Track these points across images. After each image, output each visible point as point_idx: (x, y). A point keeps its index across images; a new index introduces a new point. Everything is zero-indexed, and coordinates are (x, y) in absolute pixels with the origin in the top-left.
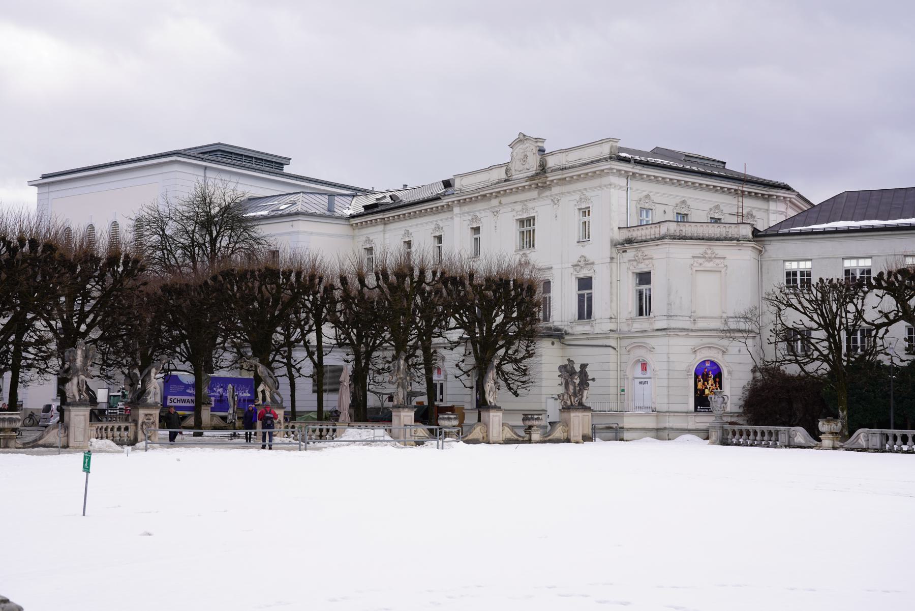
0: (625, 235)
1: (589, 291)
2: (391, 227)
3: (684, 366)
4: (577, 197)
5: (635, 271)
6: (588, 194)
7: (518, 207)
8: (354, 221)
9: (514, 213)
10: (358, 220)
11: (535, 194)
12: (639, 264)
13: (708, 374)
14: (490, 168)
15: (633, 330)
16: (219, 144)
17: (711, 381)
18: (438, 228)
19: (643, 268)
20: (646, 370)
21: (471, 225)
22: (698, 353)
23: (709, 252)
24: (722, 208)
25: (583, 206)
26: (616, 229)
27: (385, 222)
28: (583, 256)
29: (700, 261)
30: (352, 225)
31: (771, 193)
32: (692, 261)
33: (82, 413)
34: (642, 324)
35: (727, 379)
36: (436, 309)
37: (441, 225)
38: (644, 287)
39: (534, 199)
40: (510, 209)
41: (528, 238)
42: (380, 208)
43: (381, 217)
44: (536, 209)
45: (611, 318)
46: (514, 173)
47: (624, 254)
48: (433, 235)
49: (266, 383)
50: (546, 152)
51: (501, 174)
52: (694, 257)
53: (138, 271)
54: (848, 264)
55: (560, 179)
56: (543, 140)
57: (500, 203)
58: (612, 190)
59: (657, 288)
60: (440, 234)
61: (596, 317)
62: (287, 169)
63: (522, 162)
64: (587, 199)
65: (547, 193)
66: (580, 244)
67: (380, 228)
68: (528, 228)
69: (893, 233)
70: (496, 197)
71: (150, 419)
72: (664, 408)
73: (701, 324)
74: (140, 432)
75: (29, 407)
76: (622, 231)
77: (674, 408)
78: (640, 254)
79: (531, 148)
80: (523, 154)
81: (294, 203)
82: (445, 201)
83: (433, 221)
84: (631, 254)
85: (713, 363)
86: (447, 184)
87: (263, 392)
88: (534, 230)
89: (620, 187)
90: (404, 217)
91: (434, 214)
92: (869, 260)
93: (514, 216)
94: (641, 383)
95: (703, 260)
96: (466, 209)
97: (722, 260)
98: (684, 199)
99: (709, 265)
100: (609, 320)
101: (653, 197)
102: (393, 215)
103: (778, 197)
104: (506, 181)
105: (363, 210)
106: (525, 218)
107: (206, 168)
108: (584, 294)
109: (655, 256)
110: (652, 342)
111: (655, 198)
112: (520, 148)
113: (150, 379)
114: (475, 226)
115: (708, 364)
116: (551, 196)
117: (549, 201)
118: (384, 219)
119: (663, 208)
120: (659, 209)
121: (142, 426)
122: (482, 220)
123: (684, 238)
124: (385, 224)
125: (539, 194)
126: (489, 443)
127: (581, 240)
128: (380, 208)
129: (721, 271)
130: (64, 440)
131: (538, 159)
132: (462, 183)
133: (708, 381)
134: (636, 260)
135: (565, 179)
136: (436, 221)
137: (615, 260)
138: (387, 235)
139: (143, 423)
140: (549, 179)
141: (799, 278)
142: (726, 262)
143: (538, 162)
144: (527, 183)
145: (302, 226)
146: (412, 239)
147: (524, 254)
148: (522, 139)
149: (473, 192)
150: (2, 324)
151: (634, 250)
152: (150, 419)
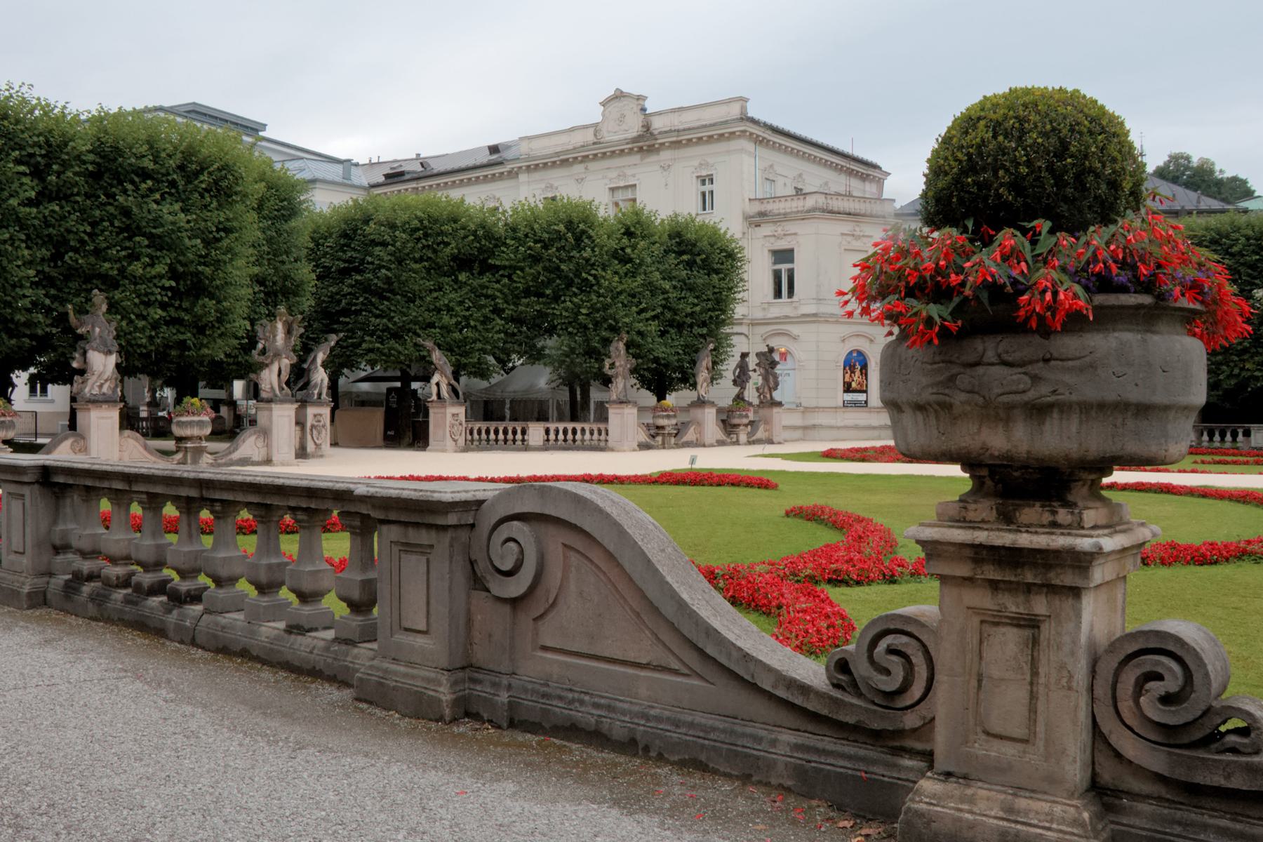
0: (756, 208)
1: (789, 266)
4: (696, 163)
6: (710, 161)
7: (614, 174)
11: (636, 158)
13: (855, 365)
14: (572, 130)
15: (770, 316)
16: (194, 103)
17: (858, 373)
19: (782, 245)
22: (846, 342)
23: (857, 229)
25: (704, 173)
26: (747, 200)
29: (849, 239)
33: (286, 413)
34: (782, 308)
36: (88, 300)
38: (784, 267)
43: (414, 185)
46: (606, 134)
49: (443, 373)
51: (589, 137)
55: (672, 143)
56: (643, 98)
59: (801, 268)
62: (261, 133)
64: (707, 164)
70: (581, 162)
72: (813, 403)
74: (309, 437)
76: (753, 203)
77: (823, 403)
78: (779, 229)
79: (630, 108)
84: (767, 230)
85: (860, 353)
86: (494, 149)
87: (438, 384)
96: (537, 176)
101: (776, 167)
102: (788, 144)
103: (874, 177)
104: (594, 144)
105: (382, 179)
110: (794, 329)
111: (778, 169)
112: (615, 107)
113: (316, 368)
115: (855, 354)
118: (417, 188)
120: (780, 181)
121: (311, 430)
123: (831, 212)
125: (642, 159)
126: (704, 446)
128: (407, 177)
130: (263, 452)
133: (854, 373)
135: (680, 141)
139: (313, 426)
140: (659, 141)
148: (619, 96)
150: (855, 266)
152: (319, 421)
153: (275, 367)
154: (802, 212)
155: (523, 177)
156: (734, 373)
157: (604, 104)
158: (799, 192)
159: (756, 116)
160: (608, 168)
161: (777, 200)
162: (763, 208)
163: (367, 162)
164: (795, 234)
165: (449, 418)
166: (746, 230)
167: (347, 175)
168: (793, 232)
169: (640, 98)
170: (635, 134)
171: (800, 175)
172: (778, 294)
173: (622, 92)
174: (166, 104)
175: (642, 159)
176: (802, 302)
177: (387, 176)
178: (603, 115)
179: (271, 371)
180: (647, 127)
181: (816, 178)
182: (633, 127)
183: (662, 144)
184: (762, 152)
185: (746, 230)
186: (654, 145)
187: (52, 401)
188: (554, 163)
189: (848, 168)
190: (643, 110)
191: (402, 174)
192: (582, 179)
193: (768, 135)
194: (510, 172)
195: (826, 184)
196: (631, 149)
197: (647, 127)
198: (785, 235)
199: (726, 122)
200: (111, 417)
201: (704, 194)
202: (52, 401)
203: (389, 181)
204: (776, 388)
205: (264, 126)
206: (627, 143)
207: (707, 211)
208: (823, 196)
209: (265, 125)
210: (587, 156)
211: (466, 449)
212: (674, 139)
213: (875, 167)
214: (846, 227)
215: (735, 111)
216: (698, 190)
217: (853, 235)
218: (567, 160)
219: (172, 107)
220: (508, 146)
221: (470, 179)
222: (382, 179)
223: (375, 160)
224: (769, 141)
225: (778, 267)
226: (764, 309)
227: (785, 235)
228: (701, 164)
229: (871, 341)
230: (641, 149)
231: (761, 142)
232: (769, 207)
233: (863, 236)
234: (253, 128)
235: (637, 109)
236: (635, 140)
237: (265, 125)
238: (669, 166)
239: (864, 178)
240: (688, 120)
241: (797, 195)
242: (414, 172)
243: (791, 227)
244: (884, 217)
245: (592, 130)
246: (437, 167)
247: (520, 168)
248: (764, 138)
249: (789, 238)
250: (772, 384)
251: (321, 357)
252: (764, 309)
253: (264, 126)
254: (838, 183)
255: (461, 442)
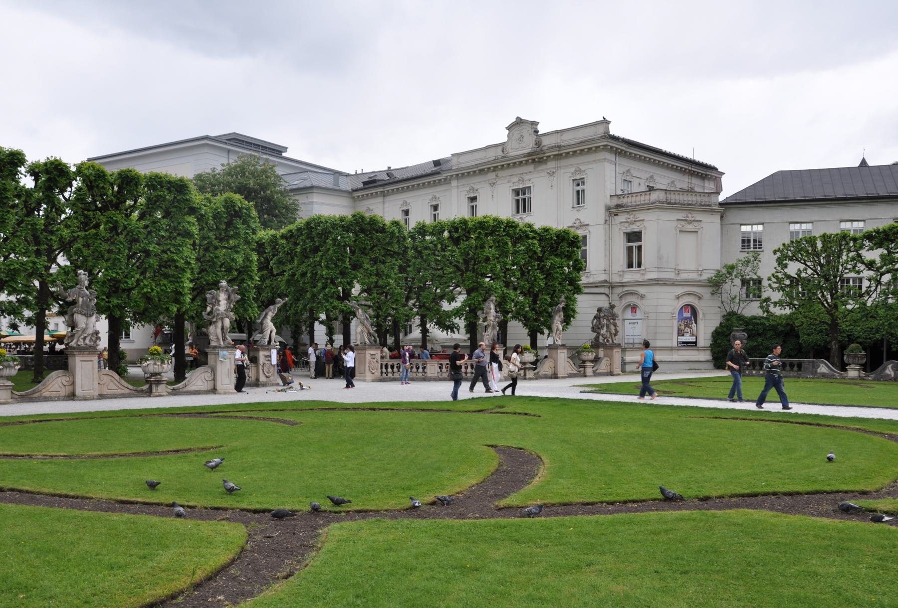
0: (615, 201)
1: (638, 244)
2: (388, 198)
3: (670, 310)
4: (573, 170)
5: (626, 231)
6: (583, 168)
7: (515, 179)
8: (356, 194)
9: (511, 184)
10: (359, 194)
11: (531, 168)
12: (631, 225)
14: (488, 147)
15: (624, 280)
16: (235, 133)
18: (405, 203)
19: (634, 228)
20: (635, 312)
21: (573, 177)
22: (680, 299)
23: (690, 216)
24: (676, 183)
25: (578, 177)
26: (609, 197)
27: (384, 195)
28: (578, 219)
29: (683, 223)
30: (354, 198)
31: (708, 173)
32: (676, 224)
34: (632, 276)
35: (702, 320)
37: (438, 196)
38: (634, 245)
39: (530, 172)
40: (506, 181)
41: (523, 203)
42: (378, 184)
43: (382, 190)
44: (586, 172)
45: (605, 270)
46: (510, 151)
47: (615, 217)
48: (430, 204)
50: (539, 133)
51: (499, 153)
52: (678, 220)
53: (179, 235)
54: (793, 227)
55: (555, 155)
57: (497, 176)
58: (606, 163)
59: (647, 243)
60: (475, 195)
61: (591, 269)
62: (284, 154)
63: (518, 141)
65: (543, 167)
66: (575, 209)
67: (380, 199)
68: (523, 197)
69: (832, 202)
70: (494, 171)
71: (374, 359)
73: (683, 276)
74: (261, 372)
75: (658, 346)
76: (613, 198)
78: (631, 217)
79: (527, 131)
80: (519, 135)
81: (305, 179)
82: (444, 175)
83: (575, 164)
84: (622, 218)
86: (437, 163)
88: (583, 191)
89: (611, 162)
90: (402, 191)
91: (432, 187)
92: (810, 225)
93: (511, 187)
94: (631, 323)
95: (685, 222)
96: (463, 181)
97: (699, 223)
98: (652, 174)
99: (690, 227)
100: (603, 272)
101: (632, 172)
103: (712, 176)
105: (361, 185)
106: (521, 189)
107: (229, 151)
108: (633, 247)
109: (646, 219)
110: (642, 290)
112: (516, 133)
114: (472, 195)
116: (547, 169)
117: (546, 174)
118: (384, 192)
119: (638, 180)
120: (635, 182)
122: (479, 191)
124: (384, 196)
125: (535, 168)
127: (575, 206)
128: (378, 184)
129: (697, 232)
131: (534, 139)
132: (459, 160)
134: (628, 222)
136: (578, 164)
137: (608, 222)
138: (386, 205)
141: (752, 243)
142: (702, 224)
143: (534, 141)
144: (525, 159)
145: (316, 198)
146: (409, 208)
147: (520, 218)
148: (519, 122)
149: (472, 167)
151: (626, 214)
153: (219, 324)
154: (648, 204)
155: (454, 183)
156: (592, 323)
157: (509, 128)
158: (651, 189)
159: (617, 134)
160: (511, 175)
161: (634, 195)
162: (620, 202)
163: (354, 173)
164: (643, 220)
165: (368, 357)
166: (607, 218)
167: (336, 182)
168: (642, 219)
169: (534, 124)
170: (529, 150)
171: (652, 177)
172: (630, 265)
173: (521, 119)
174: (213, 134)
175: (535, 168)
176: (647, 270)
177: (365, 183)
178: (508, 136)
179: (216, 327)
180: (538, 144)
181: (663, 179)
182: (528, 145)
183: (549, 156)
184: (621, 161)
185: (607, 218)
186: (542, 158)
187: (133, 342)
188: (475, 172)
189: (690, 171)
190: (536, 132)
191: (374, 181)
192: (494, 184)
193: (624, 147)
194: (445, 179)
195: (673, 182)
196: (527, 161)
197: (538, 144)
198: (635, 221)
199: (593, 140)
200: (92, 361)
201: (578, 192)
202: (133, 342)
203: (366, 186)
204: (616, 335)
205: (285, 149)
206: (525, 157)
207: (580, 205)
208: (664, 192)
209: (287, 148)
210: (497, 167)
211: (381, 380)
212: (557, 153)
213: (714, 169)
214: (681, 215)
215: (600, 130)
216: (574, 189)
217: (686, 220)
218: (483, 170)
219: (217, 137)
220: (446, 161)
221: (419, 185)
222: (361, 185)
223: (359, 172)
224: (626, 152)
225: (630, 244)
226: (620, 275)
227: (635, 221)
228: (576, 171)
229: (700, 298)
230: (534, 160)
231: (620, 153)
232: (624, 201)
233: (694, 221)
234: (277, 151)
235: (531, 131)
236: (529, 154)
237: (287, 148)
238: (554, 172)
239: (703, 177)
240: (567, 139)
241: (650, 191)
242: (383, 180)
243: (640, 216)
244: (710, 206)
245: (500, 148)
246: (399, 176)
247: (452, 176)
248: (622, 150)
249: (638, 224)
250: (613, 331)
251: (269, 318)
252: (620, 275)
253: (285, 149)
254: (682, 182)
255: (378, 374)
